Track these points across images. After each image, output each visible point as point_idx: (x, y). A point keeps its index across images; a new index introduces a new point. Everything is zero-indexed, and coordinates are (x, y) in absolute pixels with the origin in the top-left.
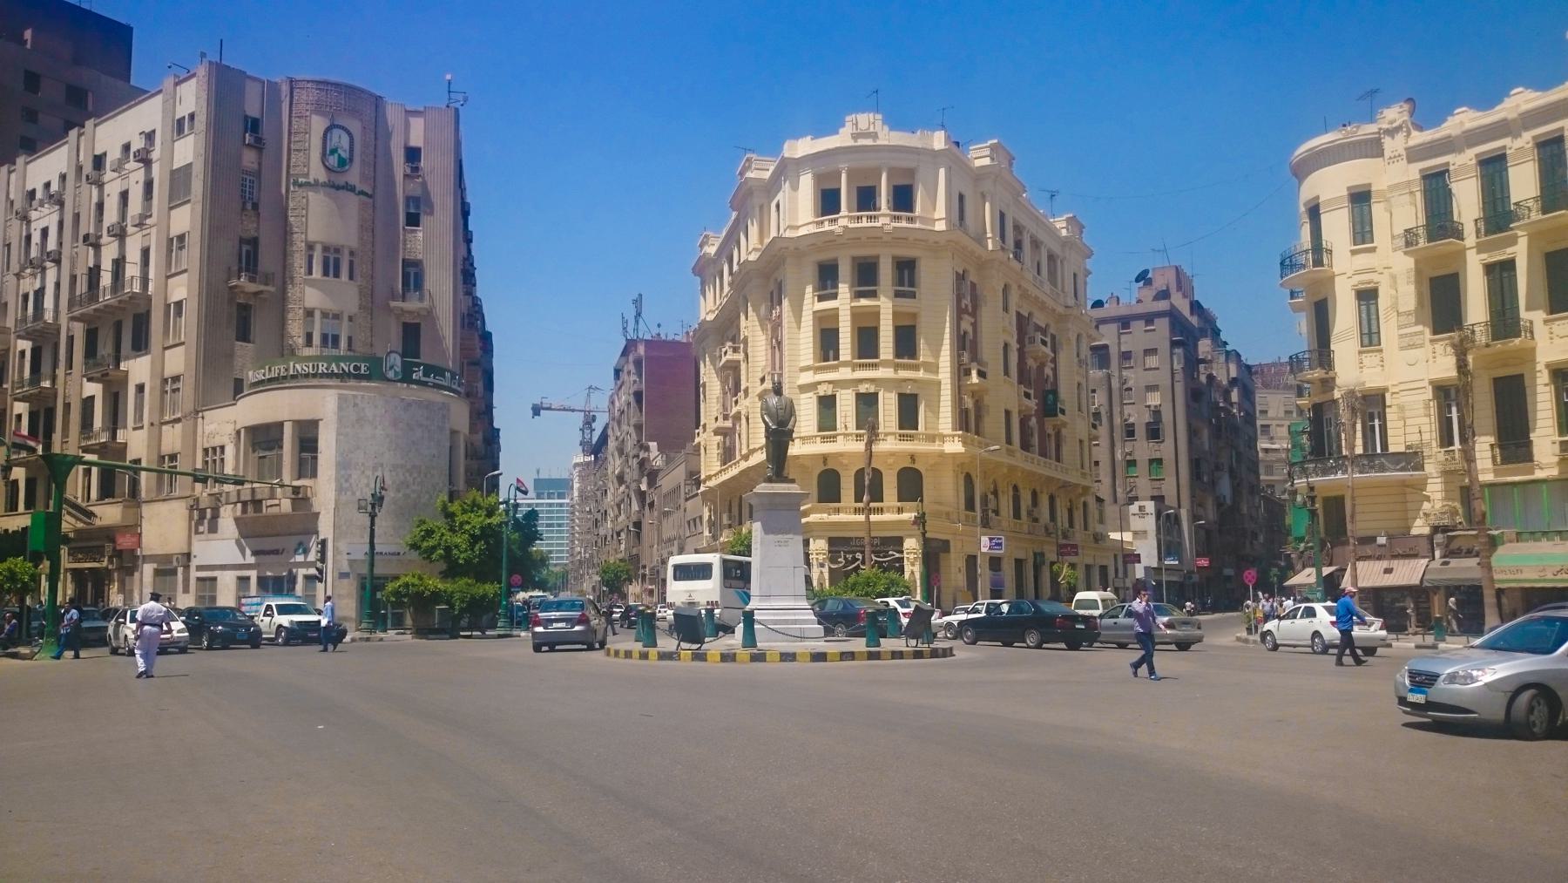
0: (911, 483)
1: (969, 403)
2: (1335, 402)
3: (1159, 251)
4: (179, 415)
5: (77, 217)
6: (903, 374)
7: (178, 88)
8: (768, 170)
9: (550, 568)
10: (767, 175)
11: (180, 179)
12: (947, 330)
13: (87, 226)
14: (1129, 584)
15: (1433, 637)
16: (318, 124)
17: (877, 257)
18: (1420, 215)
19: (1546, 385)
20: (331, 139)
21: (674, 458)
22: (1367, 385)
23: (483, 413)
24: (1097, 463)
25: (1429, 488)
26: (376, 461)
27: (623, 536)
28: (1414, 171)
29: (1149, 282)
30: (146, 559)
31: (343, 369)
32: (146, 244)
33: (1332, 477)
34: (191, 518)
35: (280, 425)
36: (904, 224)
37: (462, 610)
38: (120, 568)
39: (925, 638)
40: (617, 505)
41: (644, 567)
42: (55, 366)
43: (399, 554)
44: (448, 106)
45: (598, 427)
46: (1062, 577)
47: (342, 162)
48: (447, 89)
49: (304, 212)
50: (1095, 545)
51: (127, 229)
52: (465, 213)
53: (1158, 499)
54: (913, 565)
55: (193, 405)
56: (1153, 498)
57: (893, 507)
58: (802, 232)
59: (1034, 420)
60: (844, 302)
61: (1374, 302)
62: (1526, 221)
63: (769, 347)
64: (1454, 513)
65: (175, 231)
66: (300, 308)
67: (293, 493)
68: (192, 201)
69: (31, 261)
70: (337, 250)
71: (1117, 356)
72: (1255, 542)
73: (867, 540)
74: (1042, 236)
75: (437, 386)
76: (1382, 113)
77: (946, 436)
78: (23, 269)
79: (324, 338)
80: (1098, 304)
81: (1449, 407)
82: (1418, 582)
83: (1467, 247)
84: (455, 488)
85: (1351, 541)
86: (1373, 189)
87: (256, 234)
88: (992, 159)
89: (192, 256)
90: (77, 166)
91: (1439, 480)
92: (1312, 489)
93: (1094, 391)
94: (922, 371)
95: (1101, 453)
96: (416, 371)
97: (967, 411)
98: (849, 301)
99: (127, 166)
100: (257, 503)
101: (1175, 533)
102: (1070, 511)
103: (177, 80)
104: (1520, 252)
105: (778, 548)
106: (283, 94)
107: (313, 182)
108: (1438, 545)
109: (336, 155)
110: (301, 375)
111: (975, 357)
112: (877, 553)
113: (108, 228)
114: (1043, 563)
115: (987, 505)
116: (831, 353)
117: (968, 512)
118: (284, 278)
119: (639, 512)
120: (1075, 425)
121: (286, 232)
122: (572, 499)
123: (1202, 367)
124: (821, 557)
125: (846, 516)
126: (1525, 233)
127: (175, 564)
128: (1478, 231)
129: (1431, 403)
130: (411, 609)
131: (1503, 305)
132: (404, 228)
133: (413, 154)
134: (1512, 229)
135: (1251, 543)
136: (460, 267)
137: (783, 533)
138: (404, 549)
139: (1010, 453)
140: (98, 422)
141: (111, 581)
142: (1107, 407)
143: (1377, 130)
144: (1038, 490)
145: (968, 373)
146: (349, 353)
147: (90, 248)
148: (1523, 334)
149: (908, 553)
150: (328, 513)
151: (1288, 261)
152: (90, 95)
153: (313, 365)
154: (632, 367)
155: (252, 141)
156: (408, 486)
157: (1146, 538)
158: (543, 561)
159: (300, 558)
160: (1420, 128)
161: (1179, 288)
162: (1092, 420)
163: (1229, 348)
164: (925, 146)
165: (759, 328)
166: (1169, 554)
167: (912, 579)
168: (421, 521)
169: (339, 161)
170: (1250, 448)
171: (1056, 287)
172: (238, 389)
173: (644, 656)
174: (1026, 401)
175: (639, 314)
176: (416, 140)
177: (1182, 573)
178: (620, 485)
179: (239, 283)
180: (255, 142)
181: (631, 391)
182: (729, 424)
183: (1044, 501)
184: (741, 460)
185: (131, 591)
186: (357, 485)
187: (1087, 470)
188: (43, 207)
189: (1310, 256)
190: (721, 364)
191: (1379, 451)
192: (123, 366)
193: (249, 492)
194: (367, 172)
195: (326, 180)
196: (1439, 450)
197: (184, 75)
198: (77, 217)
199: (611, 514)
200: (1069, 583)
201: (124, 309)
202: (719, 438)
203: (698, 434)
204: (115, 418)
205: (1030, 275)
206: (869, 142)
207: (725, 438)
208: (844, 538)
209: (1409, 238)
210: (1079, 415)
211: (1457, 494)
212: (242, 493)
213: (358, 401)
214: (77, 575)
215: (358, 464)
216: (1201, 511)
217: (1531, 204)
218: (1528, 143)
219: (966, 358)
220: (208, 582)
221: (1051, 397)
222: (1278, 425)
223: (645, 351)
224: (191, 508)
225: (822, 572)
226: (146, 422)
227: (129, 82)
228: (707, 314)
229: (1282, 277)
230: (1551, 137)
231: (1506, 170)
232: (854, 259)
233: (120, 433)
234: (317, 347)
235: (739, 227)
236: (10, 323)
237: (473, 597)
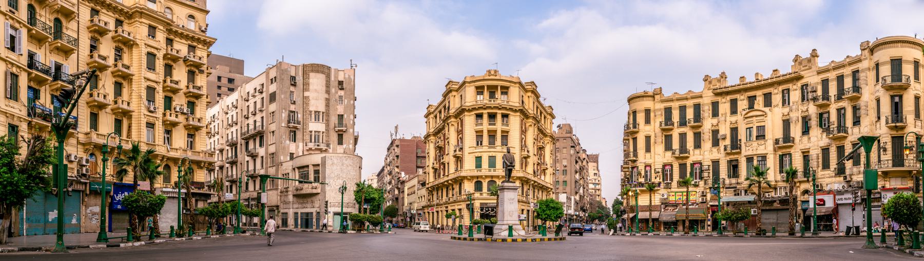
213: (332, 158)
234: (640, 111)
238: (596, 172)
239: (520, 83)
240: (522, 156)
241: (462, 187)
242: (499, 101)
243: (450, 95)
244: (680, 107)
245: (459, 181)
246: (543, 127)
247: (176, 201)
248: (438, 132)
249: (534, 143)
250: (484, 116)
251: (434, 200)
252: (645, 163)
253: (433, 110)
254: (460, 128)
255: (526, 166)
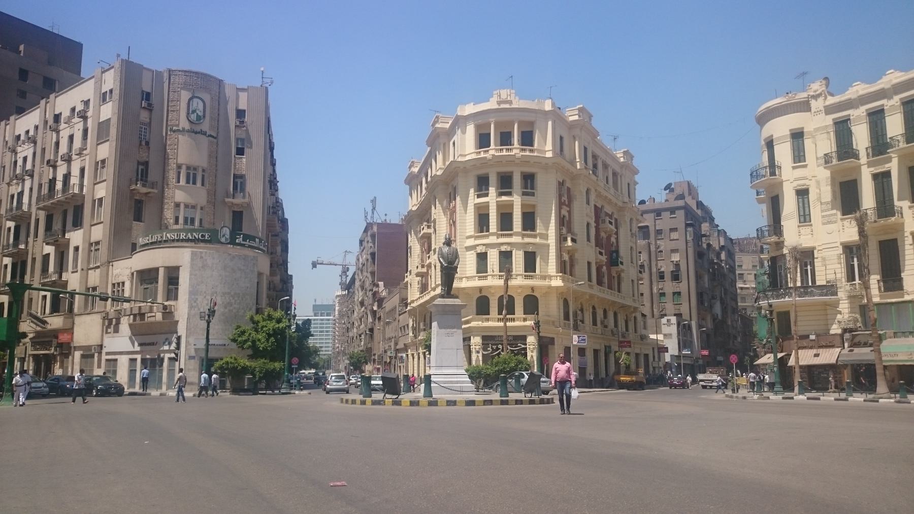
0: (531, 304)
1: (566, 257)
2: (784, 256)
3: (678, 172)
4: (99, 264)
5: (44, 150)
6: (527, 240)
7: (104, 74)
8: (448, 123)
9: (321, 356)
10: (447, 126)
11: (103, 127)
12: (553, 215)
13: (49, 155)
14: (661, 365)
15: (845, 394)
16: (185, 95)
17: (512, 173)
18: (833, 145)
19: (911, 245)
20: (192, 105)
21: (393, 291)
22: (803, 246)
23: (280, 264)
24: (642, 294)
25: (841, 306)
26: (213, 290)
27: (363, 336)
28: (829, 120)
29: (672, 190)
30: (76, 348)
32: (83, 165)
33: (782, 300)
34: (103, 324)
35: (157, 269)
36: (528, 153)
37: (260, 378)
38: (61, 354)
39: (537, 393)
40: (360, 319)
41: (375, 355)
42: (28, 236)
43: (225, 345)
44: (261, 86)
45: (350, 274)
46: (621, 360)
47: (199, 118)
48: (261, 76)
49: (176, 146)
50: (642, 342)
51: (72, 157)
52: (272, 149)
53: (679, 315)
54: (532, 352)
55: (107, 258)
56: (675, 315)
57: (520, 318)
58: (468, 158)
59: (605, 268)
60: (492, 198)
61: (806, 197)
62: (897, 148)
63: (448, 225)
64: (856, 321)
65: (100, 157)
66: (172, 202)
67: (163, 309)
68: (110, 140)
69: (16, 176)
70: (195, 169)
71: (653, 232)
72: (735, 341)
73: (505, 337)
74: (609, 161)
75: (250, 247)
76: (810, 86)
77: (553, 276)
78: (11, 180)
79: (186, 219)
80: (642, 202)
81: (853, 258)
82: (835, 362)
83: (862, 164)
84: (260, 307)
85: (795, 337)
86: (805, 130)
87: (147, 160)
88: (579, 116)
89: (109, 172)
90: (44, 121)
91: (847, 301)
92: (771, 306)
93: (640, 253)
94: (538, 238)
95: (645, 289)
96: (238, 238)
97: (565, 261)
98: (495, 198)
99: (73, 120)
100: (142, 315)
101: (689, 336)
102: (626, 322)
103: (103, 70)
104: (894, 166)
105: (448, 337)
106: (165, 79)
107: (181, 129)
108: (847, 340)
109: (195, 114)
110: (170, 240)
111: (570, 230)
112: (511, 345)
113: (61, 156)
114: (610, 352)
115: (576, 317)
116: (485, 228)
117: (566, 321)
118: (163, 182)
119: (372, 323)
120: (629, 271)
121: (165, 158)
122: (334, 316)
123: (704, 239)
124: (477, 347)
125: (493, 323)
126: (896, 155)
127: (93, 351)
128: (868, 155)
129: (842, 256)
130: (230, 377)
131: (884, 198)
132: (235, 156)
133: (240, 114)
134: (888, 153)
135: (733, 342)
136: (267, 179)
137: (450, 328)
138: (228, 342)
139: (591, 287)
140: (51, 269)
141: (56, 361)
142: (648, 261)
143: (807, 96)
144: (607, 309)
145: (565, 239)
146: (200, 228)
147: (51, 168)
148: (897, 215)
149: (529, 345)
150: (183, 321)
151: (755, 174)
152: (57, 82)
153: (177, 235)
154: (369, 239)
155: (146, 106)
156: (231, 305)
157: (671, 338)
158: (316, 351)
159: (166, 348)
160: (832, 95)
161: (690, 194)
162: (639, 269)
163: (719, 228)
164: (540, 108)
165: (442, 214)
166: (685, 347)
167: (532, 360)
168: (237, 326)
169: (197, 118)
170: (732, 286)
171: (617, 190)
172: (134, 248)
173: (363, 403)
174: (600, 257)
175: (374, 208)
176: (242, 106)
177: (692, 359)
178: (362, 307)
179: (136, 188)
180: (148, 106)
181: (369, 253)
182: (425, 270)
183: (611, 315)
184: (431, 291)
185: (67, 368)
186: (201, 304)
187: (636, 297)
188: (24, 144)
189: (768, 170)
190: (421, 235)
191: (810, 284)
192: (67, 236)
193: (137, 309)
194: (213, 124)
195: (189, 128)
196: (847, 283)
197: (107, 67)
198: (44, 150)
199: (356, 324)
200: (625, 363)
201: (69, 203)
202: (419, 278)
203: (407, 276)
204: (61, 266)
205: (602, 183)
206: (507, 106)
207: (422, 278)
208: (491, 336)
209: (827, 159)
210: (631, 265)
211: (858, 310)
212: (133, 309)
213: (203, 255)
214: (36, 358)
215: (202, 292)
216: (704, 323)
217: (899, 138)
218: (897, 102)
219: (564, 231)
220: (112, 362)
221: (614, 255)
222: (748, 274)
223: (377, 229)
224: (104, 319)
225: (478, 356)
226: (79, 268)
227: (80, 75)
228: (413, 206)
229: (751, 183)
230: (910, 99)
231: (884, 118)
232: (498, 173)
233: (64, 275)
234: (181, 224)
235: (431, 156)
236: (3, 212)
237: (267, 370)
247: (900, 114)
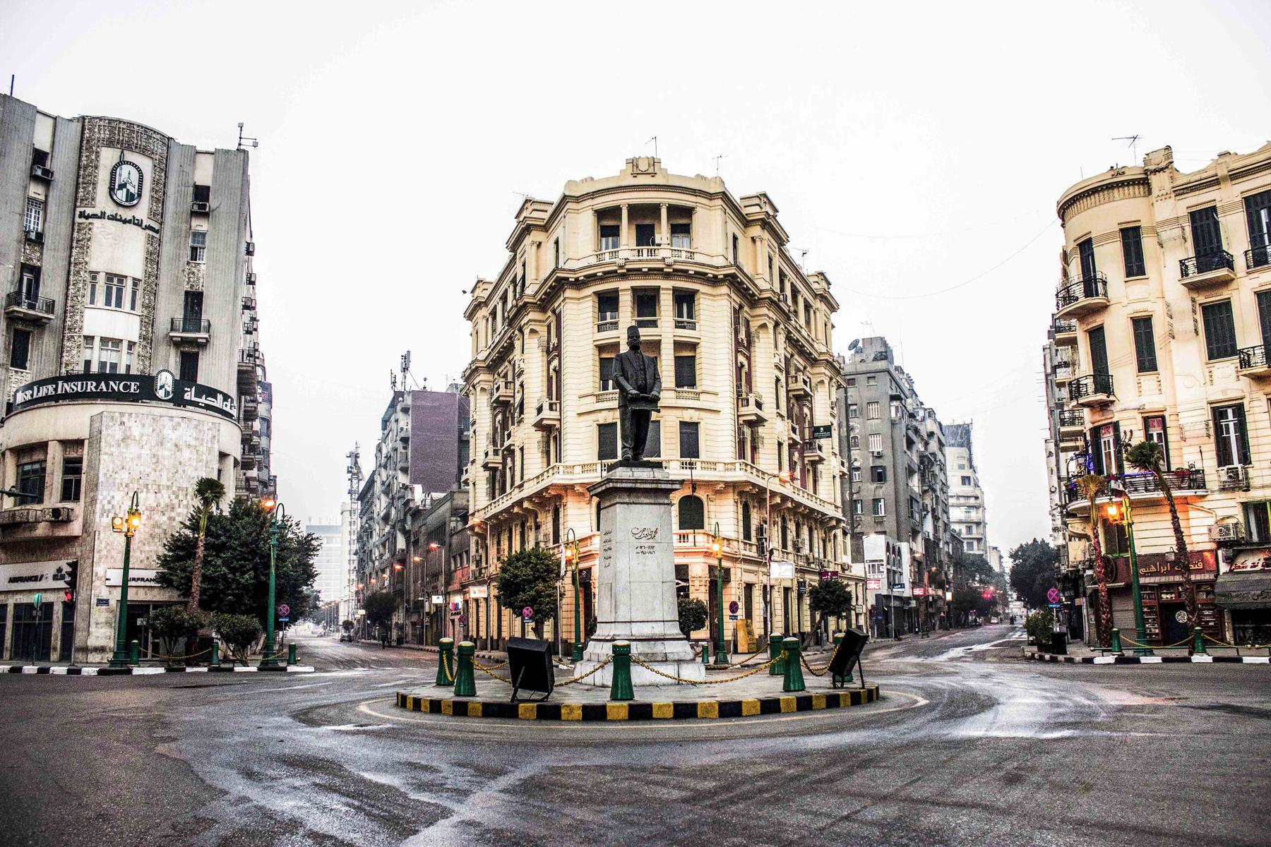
20: (120, 175)
31: (112, 388)
47: (130, 197)
75: (208, 407)
213: (125, 419)
238: (967, 473)
239: (725, 196)
240: (741, 419)
241: (561, 521)
242: (663, 253)
243: (528, 240)
244: (1246, 199)
245: (551, 501)
246: (804, 333)
248: (500, 358)
249: (778, 380)
250: (621, 298)
251: (490, 561)
252: (1140, 409)
253: (486, 294)
254: (554, 340)
255: (754, 449)
